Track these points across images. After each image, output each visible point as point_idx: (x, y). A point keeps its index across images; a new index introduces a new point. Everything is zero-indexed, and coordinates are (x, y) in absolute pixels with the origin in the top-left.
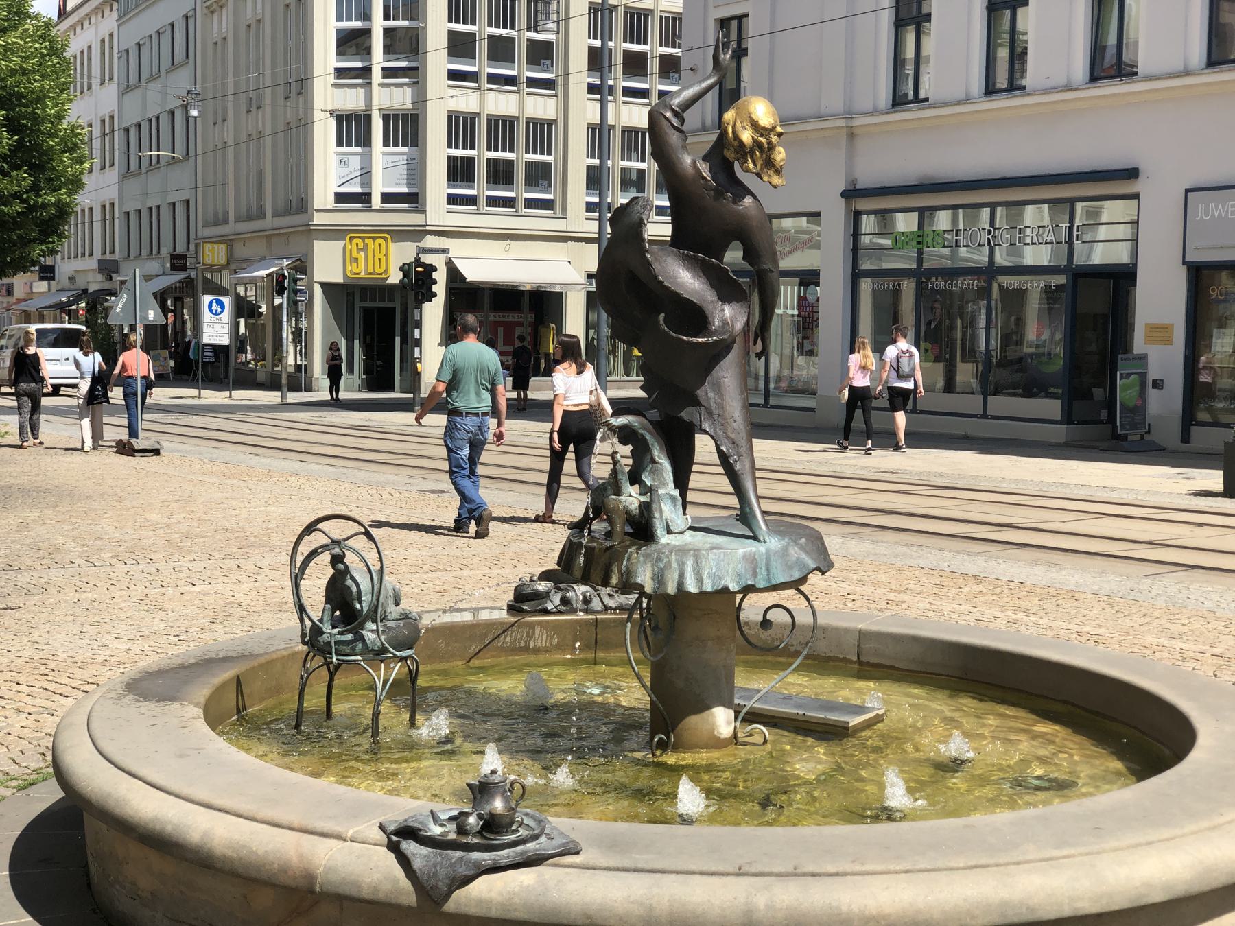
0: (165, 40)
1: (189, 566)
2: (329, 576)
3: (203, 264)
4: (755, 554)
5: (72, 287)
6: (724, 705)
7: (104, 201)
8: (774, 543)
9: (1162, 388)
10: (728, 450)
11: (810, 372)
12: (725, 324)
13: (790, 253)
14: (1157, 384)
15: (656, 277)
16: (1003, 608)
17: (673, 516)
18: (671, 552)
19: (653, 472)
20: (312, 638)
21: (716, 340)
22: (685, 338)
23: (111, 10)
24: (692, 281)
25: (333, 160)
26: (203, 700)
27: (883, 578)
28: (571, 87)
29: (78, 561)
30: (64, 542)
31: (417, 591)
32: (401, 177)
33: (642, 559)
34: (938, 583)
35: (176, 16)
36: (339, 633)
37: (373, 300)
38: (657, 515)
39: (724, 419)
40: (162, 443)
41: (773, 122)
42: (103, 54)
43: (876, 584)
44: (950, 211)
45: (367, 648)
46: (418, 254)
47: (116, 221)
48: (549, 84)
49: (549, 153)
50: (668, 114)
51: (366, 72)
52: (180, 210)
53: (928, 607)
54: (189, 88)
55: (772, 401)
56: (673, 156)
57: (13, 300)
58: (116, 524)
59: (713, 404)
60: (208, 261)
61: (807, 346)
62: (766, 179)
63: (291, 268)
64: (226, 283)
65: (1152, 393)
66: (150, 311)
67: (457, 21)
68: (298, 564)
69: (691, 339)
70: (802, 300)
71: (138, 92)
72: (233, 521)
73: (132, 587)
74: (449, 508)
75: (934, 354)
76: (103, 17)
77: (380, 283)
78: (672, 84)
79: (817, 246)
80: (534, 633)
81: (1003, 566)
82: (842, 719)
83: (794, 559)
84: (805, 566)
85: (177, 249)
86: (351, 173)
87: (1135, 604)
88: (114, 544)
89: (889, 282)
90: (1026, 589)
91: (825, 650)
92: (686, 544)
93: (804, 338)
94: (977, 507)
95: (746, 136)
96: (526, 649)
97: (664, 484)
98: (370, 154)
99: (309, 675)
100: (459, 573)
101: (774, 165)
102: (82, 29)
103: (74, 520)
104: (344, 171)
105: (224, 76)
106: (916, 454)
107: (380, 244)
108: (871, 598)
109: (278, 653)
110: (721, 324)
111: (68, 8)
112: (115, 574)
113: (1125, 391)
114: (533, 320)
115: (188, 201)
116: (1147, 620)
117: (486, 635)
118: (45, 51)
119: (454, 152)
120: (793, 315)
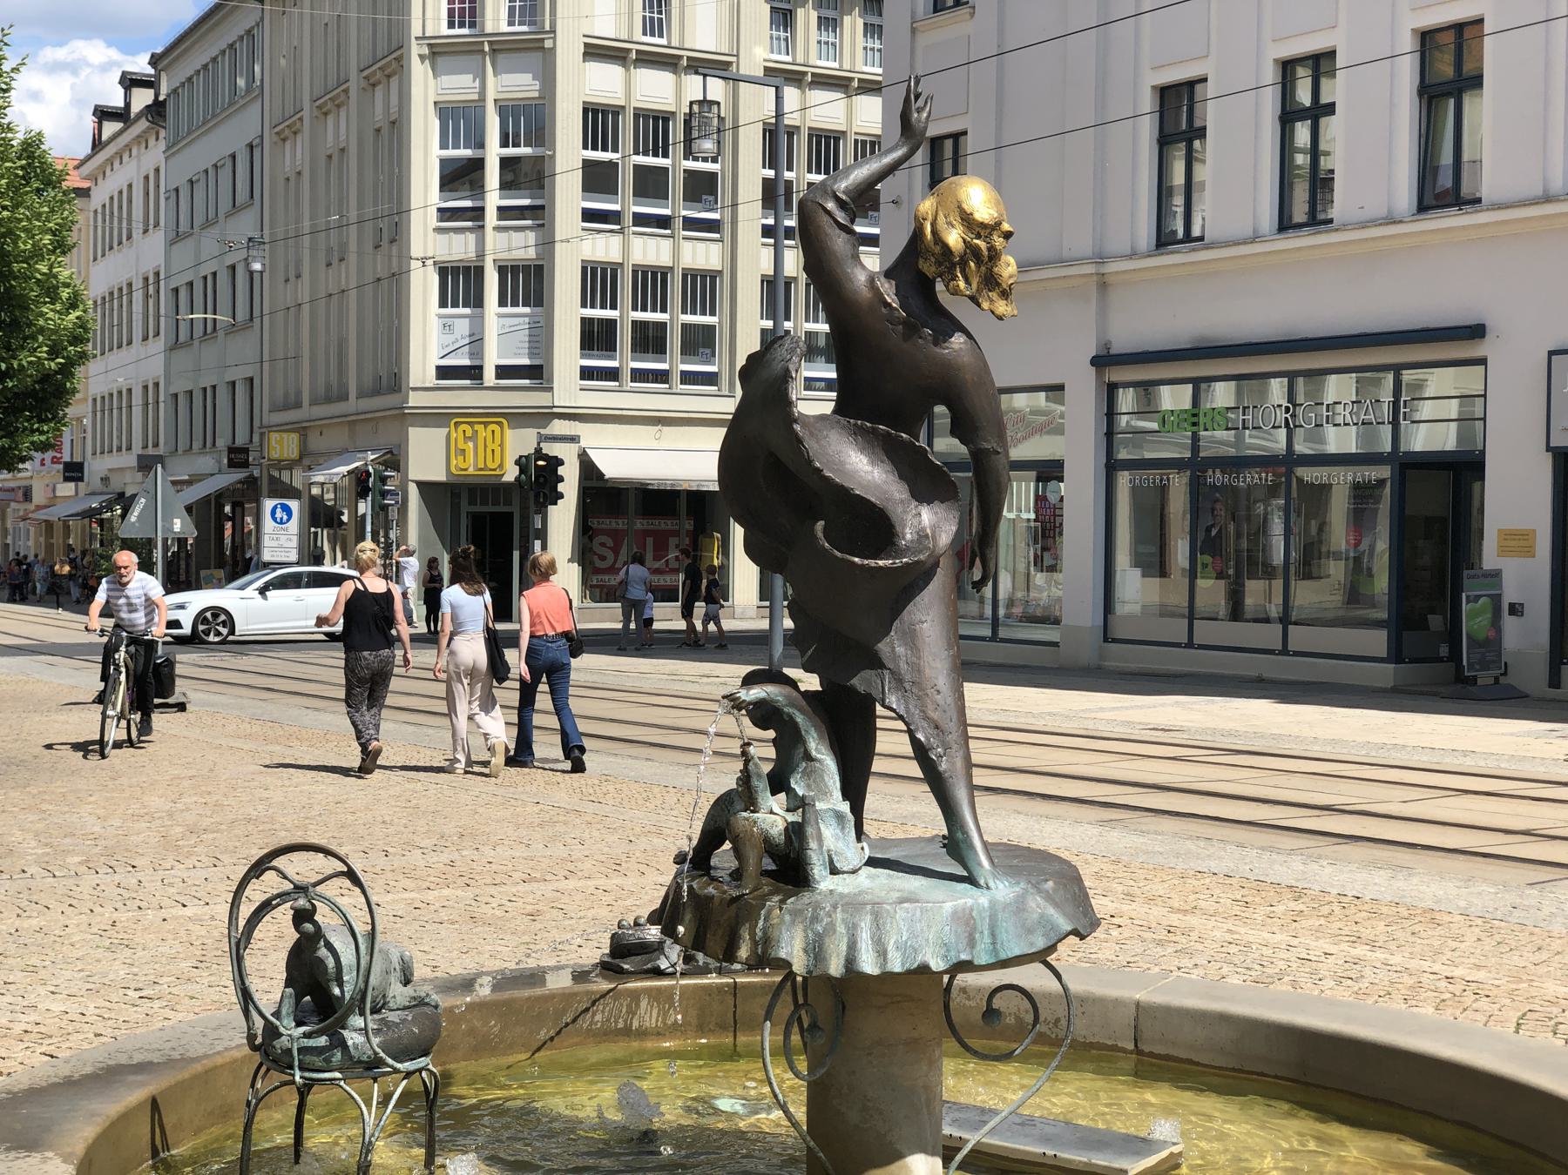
0: (225, 173)
1: (185, 876)
2: (290, 945)
3: (269, 460)
4: (972, 909)
5: (105, 490)
6: (925, 1151)
7: (147, 381)
8: (1003, 890)
9: (1522, 615)
10: (926, 737)
11: (1051, 594)
12: (922, 536)
13: (1025, 438)
14: (1515, 610)
15: (810, 462)
16: (1336, 937)
17: (840, 844)
18: (835, 907)
19: (807, 774)
20: (266, 1047)
21: (906, 563)
22: (856, 559)
23: (157, 139)
24: (868, 468)
25: (434, 324)
26: (79, 1148)
27: (1160, 889)
28: (740, 225)
29: (33, 870)
30: (20, 840)
31: (499, 913)
32: (520, 345)
33: (787, 918)
34: (1239, 897)
35: (239, 147)
36: (307, 1035)
37: (484, 502)
38: (813, 845)
39: (921, 689)
40: (189, 693)
41: (996, 215)
42: (147, 194)
43: (1150, 900)
44: (1233, 383)
45: (351, 1058)
46: (539, 444)
47: (162, 405)
48: (712, 226)
49: (713, 313)
50: (830, 205)
51: (478, 213)
52: (241, 391)
53: (1228, 937)
54: (251, 234)
55: (1003, 633)
56: (838, 271)
57: (32, 507)
58: (101, 812)
59: (903, 666)
60: (275, 455)
61: (1048, 561)
62: (985, 305)
63: (379, 463)
64: (297, 483)
65: (1509, 623)
66: (175, 520)
67: (595, 148)
68: (242, 923)
69: (866, 562)
70: (1040, 500)
71: (190, 242)
72: (260, 808)
73: (97, 909)
74: (562, 785)
75: (1216, 570)
76: (147, 147)
77: (493, 481)
78: (870, 225)
79: (1059, 430)
80: (638, 1006)
81: (1329, 870)
82: (1116, 1165)
83: (1035, 916)
84: (1054, 927)
85: (237, 442)
86: (457, 340)
87: (1522, 931)
88: (89, 842)
89: (1153, 475)
90: (1366, 907)
91: (1083, 1033)
92: (860, 893)
93: (1044, 549)
94: (1283, 780)
95: (954, 238)
96: (627, 1032)
97: (825, 793)
98: (482, 317)
99: (259, 1101)
100: (563, 885)
101: (999, 285)
102: (121, 163)
103: (45, 806)
104: (450, 339)
105: (298, 220)
106: (1195, 703)
107: (493, 431)
108: (1145, 923)
109: (226, 1054)
110: (916, 537)
111: (104, 137)
112: (79, 889)
113: (1473, 617)
114: (692, 528)
115: (251, 379)
116: (1544, 956)
117: (564, 1011)
118: (20, 173)
119: (590, 312)
120: (1029, 520)
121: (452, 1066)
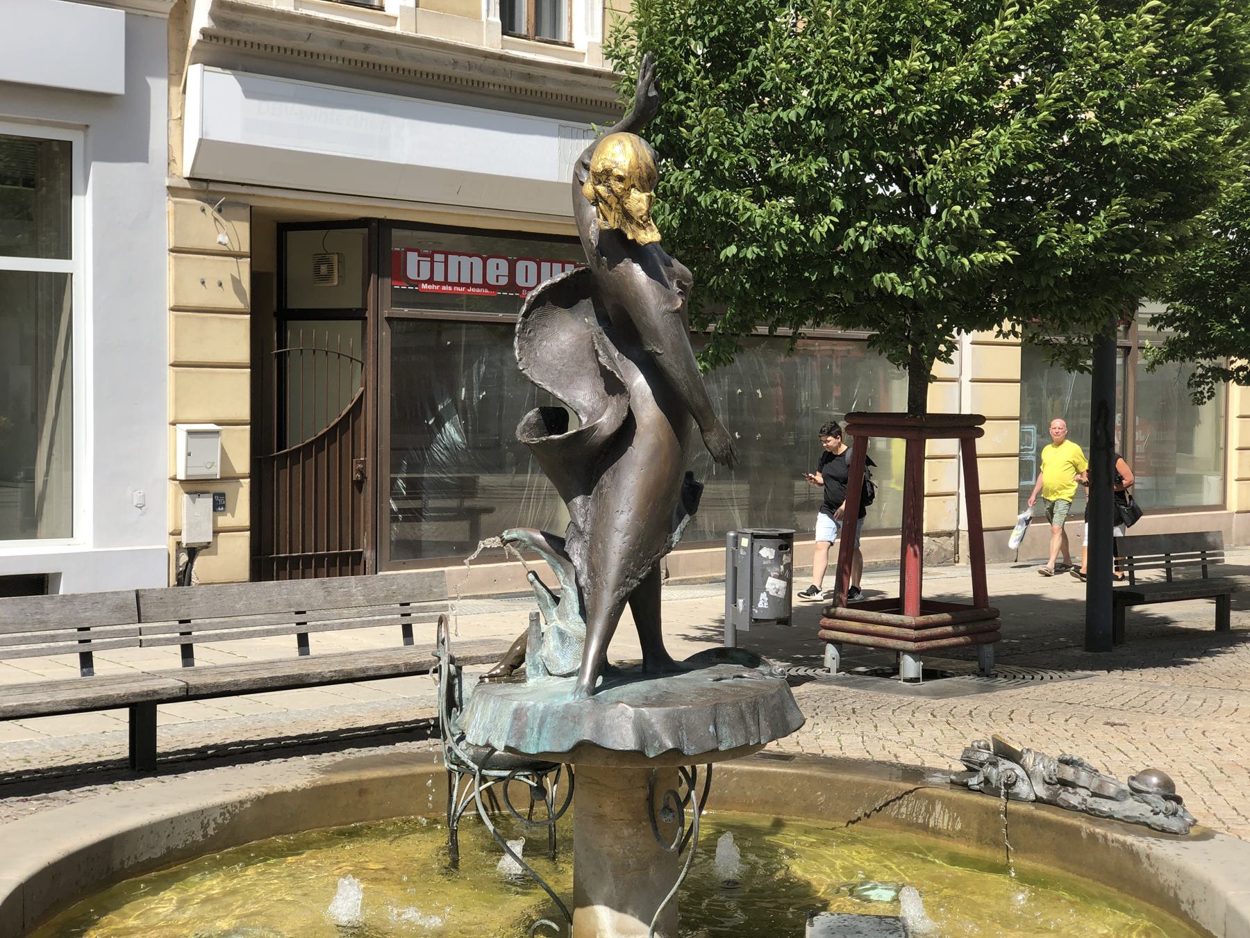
80: (934, 809)
92: (308, 675)
94: (282, 534)
96: (924, 827)
115: (190, 433)
117: (877, 799)
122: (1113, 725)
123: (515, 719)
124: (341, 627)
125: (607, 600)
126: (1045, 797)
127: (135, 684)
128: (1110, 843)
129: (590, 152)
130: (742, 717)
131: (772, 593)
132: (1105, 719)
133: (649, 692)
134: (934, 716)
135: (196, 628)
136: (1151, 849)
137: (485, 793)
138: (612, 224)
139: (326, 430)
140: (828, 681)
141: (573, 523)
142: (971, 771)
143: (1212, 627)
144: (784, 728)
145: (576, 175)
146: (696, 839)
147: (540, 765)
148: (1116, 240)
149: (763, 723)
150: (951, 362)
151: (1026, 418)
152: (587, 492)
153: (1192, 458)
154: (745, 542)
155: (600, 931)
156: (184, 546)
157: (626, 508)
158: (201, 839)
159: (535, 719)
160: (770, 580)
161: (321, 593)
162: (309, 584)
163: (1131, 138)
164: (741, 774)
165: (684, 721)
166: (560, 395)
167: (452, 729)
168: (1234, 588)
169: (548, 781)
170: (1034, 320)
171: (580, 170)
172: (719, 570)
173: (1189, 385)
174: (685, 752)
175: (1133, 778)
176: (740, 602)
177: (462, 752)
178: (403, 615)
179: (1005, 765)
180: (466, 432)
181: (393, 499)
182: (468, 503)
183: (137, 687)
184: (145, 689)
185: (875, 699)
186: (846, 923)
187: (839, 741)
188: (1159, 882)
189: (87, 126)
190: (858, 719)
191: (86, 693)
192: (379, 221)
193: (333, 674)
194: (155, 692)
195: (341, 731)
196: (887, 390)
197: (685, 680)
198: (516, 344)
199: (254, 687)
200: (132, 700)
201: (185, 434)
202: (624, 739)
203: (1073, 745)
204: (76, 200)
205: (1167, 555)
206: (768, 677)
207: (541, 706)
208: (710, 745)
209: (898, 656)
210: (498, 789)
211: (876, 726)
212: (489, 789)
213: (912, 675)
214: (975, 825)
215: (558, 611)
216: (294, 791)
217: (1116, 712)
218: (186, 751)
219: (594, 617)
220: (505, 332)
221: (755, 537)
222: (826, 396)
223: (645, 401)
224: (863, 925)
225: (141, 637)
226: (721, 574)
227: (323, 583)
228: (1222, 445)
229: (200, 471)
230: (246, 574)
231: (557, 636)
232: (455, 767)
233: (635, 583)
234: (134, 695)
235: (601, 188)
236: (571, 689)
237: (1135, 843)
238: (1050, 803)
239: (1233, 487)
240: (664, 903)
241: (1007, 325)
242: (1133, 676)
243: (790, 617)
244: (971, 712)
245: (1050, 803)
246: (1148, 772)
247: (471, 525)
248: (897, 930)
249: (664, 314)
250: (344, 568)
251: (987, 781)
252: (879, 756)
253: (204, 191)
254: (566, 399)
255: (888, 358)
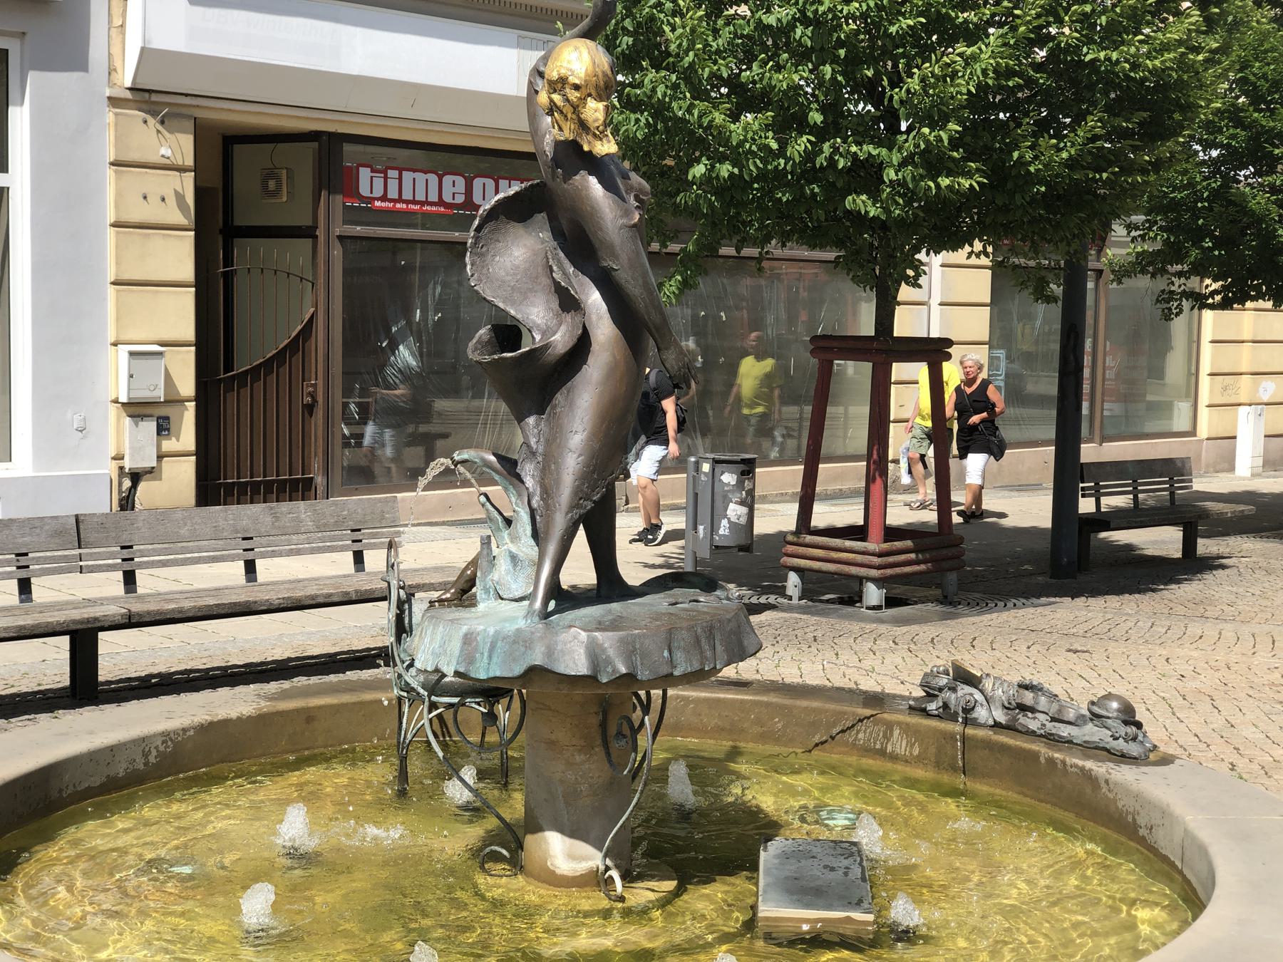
80: (892, 734)
92: (256, 602)
96: (882, 753)
115: (132, 354)
117: (834, 725)
121: (742, 744)
122: (1076, 652)
123: (465, 643)
124: (290, 553)
125: (560, 522)
126: (1004, 722)
127: (74, 611)
128: (1068, 768)
129: (545, 59)
130: (697, 641)
131: (734, 519)
132: (1068, 646)
133: (603, 616)
134: (896, 644)
135: (138, 554)
136: (1110, 774)
137: (436, 721)
138: (568, 134)
139: (274, 352)
140: (790, 609)
141: (526, 444)
142: (930, 696)
143: (1179, 555)
144: (740, 653)
145: (530, 83)
146: (649, 765)
147: (492, 692)
148: (1096, 159)
149: (719, 648)
150: (920, 286)
151: (995, 343)
152: (540, 412)
153: (1164, 385)
154: (706, 467)
155: (551, 856)
156: (127, 471)
157: (580, 428)
158: (142, 767)
159: (486, 643)
160: (732, 506)
161: (269, 519)
162: (257, 509)
163: (1115, 56)
164: (698, 701)
165: (638, 646)
166: (513, 312)
167: (402, 656)
168: (1204, 515)
169: (500, 708)
170: (1006, 242)
171: (535, 78)
172: (680, 497)
173: (1158, 301)
174: (639, 677)
175: (1093, 703)
176: (701, 528)
177: (412, 679)
178: (354, 541)
179: (964, 690)
180: (421, 355)
181: (346, 424)
182: (423, 428)
183: (76, 615)
184: (86, 616)
185: (837, 626)
186: (801, 848)
187: (799, 669)
188: (1117, 808)
189: (24, 33)
190: (819, 647)
191: (24, 620)
192: (330, 134)
193: (281, 601)
194: (96, 619)
195: (290, 659)
196: (855, 313)
197: (639, 604)
198: (467, 259)
199: (200, 614)
200: (74, 627)
201: (127, 355)
202: (577, 664)
203: (1035, 672)
204: (12, 111)
205: (1135, 481)
206: (725, 602)
207: (491, 631)
208: (664, 670)
209: (861, 584)
210: (449, 716)
211: (837, 654)
212: (440, 716)
213: (874, 602)
214: (933, 750)
215: (509, 534)
216: (239, 718)
217: (1079, 639)
218: (129, 679)
219: (546, 540)
220: (458, 249)
221: (716, 462)
222: (792, 319)
223: (600, 318)
224: (816, 850)
225: (81, 563)
226: (682, 501)
227: (272, 508)
228: (1193, 371)
229: (143, 394)
230: (193, 501)
231: (509, 559)
232: (405, 694)
233: (589, 505)
234: (74, 622)
235: (556, 97)
236: (523, 613)
237: (1094, 768)
238: (1010, 728)
239: (1203, 413)
240: (616, 829)
241: (978, 246)
242: (1097, 603)
243: (752, 543)
244: (933, 639)
245: (1010, 728)
246: (1109, 697)
247: (427, 450)
248: (852, 855)
249: (621, 229)
250: (294, 494)
251: (946, 706)
252: (838, 682)
253: (146, 102)
254: (519, 316)
255: (852, 279)
